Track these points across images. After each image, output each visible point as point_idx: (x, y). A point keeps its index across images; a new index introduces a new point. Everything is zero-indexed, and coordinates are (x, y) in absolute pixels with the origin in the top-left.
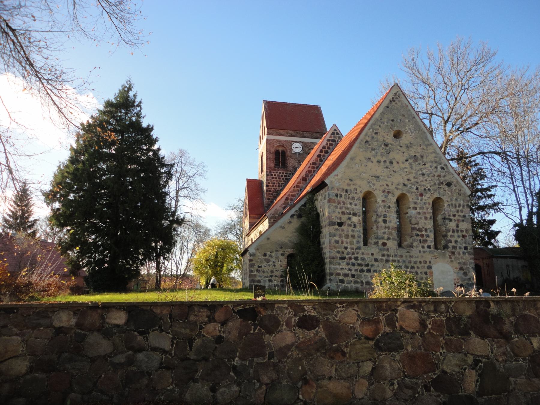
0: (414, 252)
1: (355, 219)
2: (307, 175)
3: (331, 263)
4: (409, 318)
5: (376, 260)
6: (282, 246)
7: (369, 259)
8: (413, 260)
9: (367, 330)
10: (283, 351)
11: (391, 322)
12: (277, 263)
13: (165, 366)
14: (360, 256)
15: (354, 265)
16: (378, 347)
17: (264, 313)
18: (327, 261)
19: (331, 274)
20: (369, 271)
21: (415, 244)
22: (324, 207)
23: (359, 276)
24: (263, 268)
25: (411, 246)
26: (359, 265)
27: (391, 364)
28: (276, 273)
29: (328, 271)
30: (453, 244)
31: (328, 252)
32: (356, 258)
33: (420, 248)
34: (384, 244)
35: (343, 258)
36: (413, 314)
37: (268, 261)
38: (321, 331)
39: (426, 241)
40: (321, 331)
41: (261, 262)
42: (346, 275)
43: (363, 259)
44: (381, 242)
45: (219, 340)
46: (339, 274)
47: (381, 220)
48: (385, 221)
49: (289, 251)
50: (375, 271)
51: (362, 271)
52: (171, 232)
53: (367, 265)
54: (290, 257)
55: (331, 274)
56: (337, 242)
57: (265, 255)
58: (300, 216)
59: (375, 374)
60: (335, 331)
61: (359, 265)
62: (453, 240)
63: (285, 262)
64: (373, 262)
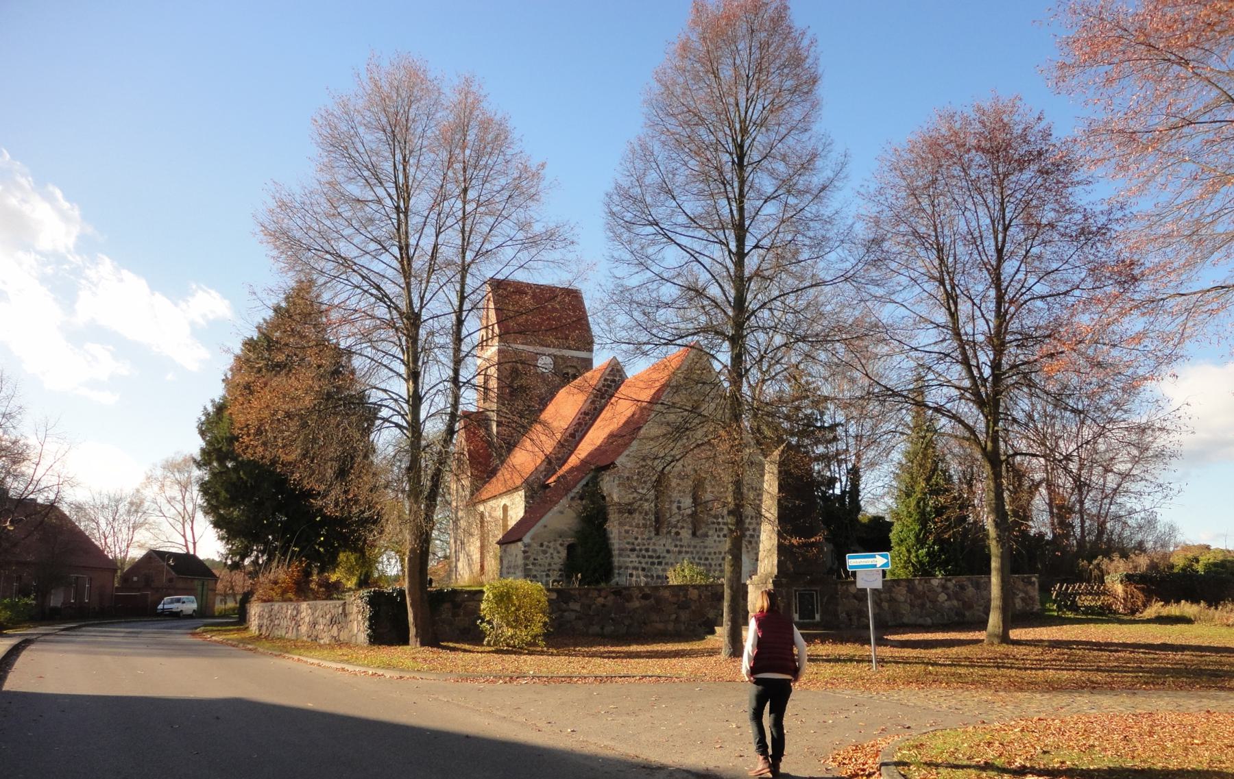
0: (709, 541)
1: (646, 506)
2: (576, 431)
3: (620, 555)
4: (694, 594)
5: (668, 551)
6: (561, 535)
7: (660, 550)
8: (707, 550)
9: (674, 600)
10: (635, 610)
11: (685, 596)
12: (555, 554)
13: (578, 618)
14: (651, 547)
15: (644, 557)
16: (679, 607)
17: (625, 592)
18: (616, 552)
19: (620, 568)
20: (660, 563)
21: (710, 533)
22: (611, 488)
23: (650, 570)
24: (540, 561)
25: (706, 535)
26: (650, 557)
27: (684, 615)
28: (554, 567)
29: (616, 564)
30: (751, 532)
31: (616, 542)
32: (647, 550)
33: (715, 537)
34: (677, 534)
35: (633, 550)
36: (696, 592)
37: (545, 552)
38: (652, 600)
39: (721, 529)
40: (652, 600)
41: (538, 554)
42: (636, 568)
43: (655, 551)
44: (674, 530)
45: (604, 605)
46: (627, 568)
47: (675, 506)
48: (679, 508)
49: (570, 540)
50: (667, 564)
51: (653, 563)
52: (272, 473)
53: (658, 557)
54: (571, 548)
55: (620, 568)
56: (627, 532)
57: (542, 545)
58: (581, 498)
59: (677, 620)
60: (659, 601)
61: (650, 557)
62: (751, 527)
63: (564, 554)
64: (665, 554)
